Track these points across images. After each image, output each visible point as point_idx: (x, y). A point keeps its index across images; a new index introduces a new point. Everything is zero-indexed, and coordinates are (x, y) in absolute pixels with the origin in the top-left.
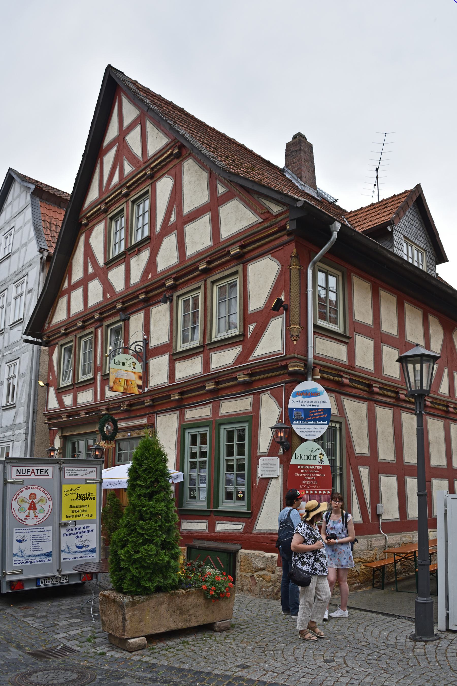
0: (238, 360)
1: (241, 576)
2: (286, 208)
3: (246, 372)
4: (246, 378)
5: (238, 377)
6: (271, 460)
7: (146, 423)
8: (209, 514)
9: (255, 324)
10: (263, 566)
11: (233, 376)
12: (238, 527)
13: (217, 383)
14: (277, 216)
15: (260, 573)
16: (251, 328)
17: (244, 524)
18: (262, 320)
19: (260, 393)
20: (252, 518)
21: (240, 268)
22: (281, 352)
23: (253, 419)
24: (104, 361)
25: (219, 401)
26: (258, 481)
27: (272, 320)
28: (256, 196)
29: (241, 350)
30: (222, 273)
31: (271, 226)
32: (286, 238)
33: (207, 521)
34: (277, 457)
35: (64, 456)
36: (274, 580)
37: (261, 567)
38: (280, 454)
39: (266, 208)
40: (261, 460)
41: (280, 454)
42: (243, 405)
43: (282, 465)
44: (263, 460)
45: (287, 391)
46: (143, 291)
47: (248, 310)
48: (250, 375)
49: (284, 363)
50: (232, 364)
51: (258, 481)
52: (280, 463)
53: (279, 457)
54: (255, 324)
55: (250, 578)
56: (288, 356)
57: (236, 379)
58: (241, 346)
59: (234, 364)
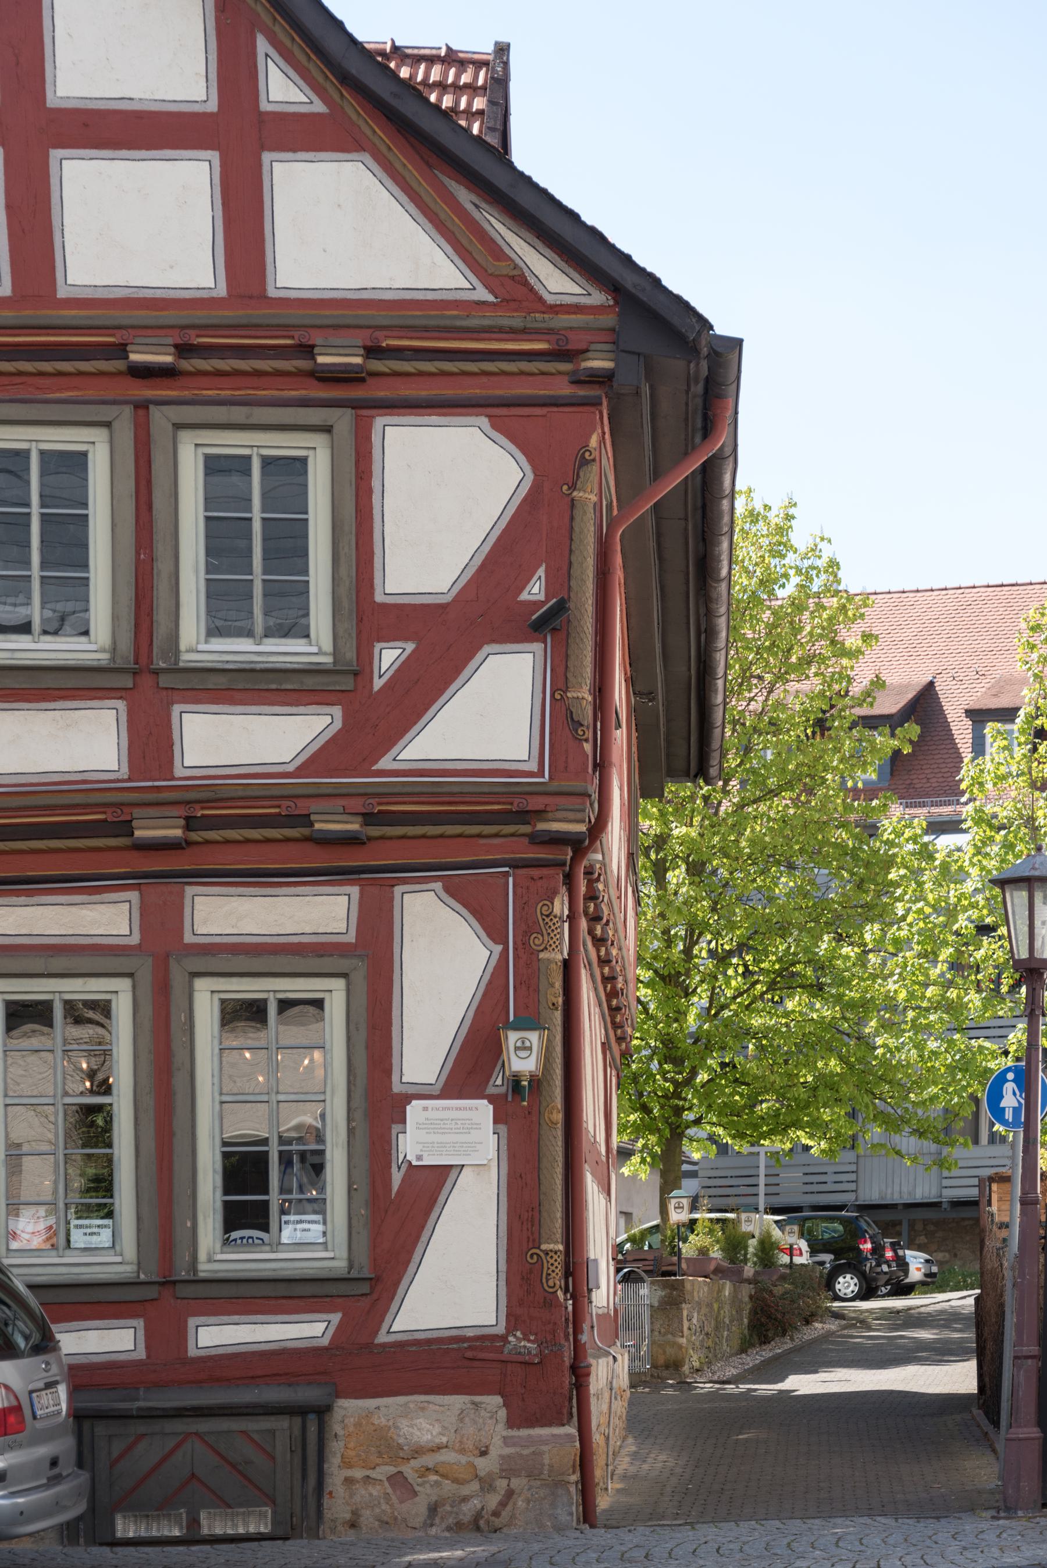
0: (322, 759)
1: (349, 1481)
2: (598, 298)
3: (357, 805)
4: (354, 826)
5: (313, 817)
6: (444, 1109)
8: (152, 1292)
9: (410, 647)
10: (444, 1440)
11: (302, 807)
12: (310, 1330)
13: (190, 823)
14: (557, 309)
15: (429, 1460)
16: (389, 657)
17: (336, 1318)
18: (448, 637)
19: (393, 886)
20: (375, 1296)
21: (343, 420)
22: (533, 766)
23: (371, 960)
24: (473, 799)
25: (180, 885)
26: (397, 1178)
27: (487, 649)
28: (465, 196)
29: (338, 724)
30: (244, 410)
31: (524, 331)
32: (565, 389)
33: (139, 1323)
34: (485, 1102)
35: (702, 1087)
36: (490, 1474)
37: (437, 1440)
38: (490, 1090)
39: (516, 267)
40: (414, 1110)
41: (490, 1090)
42: (324, 912)
43: (503, 1129)
44: (425, 1109)
45: (519, 891)
47: (372, 587)
48: (369, 818)
49: (536, 803)
50: (291, 768)
51: (397, 1178)
52: (496, 1121)
53: (491, 1099)
54: (410, 647)
55: (386, 1484)
56: (555, 786)
57: (305, 820)
58: (337, 711)
59: (302, 770)
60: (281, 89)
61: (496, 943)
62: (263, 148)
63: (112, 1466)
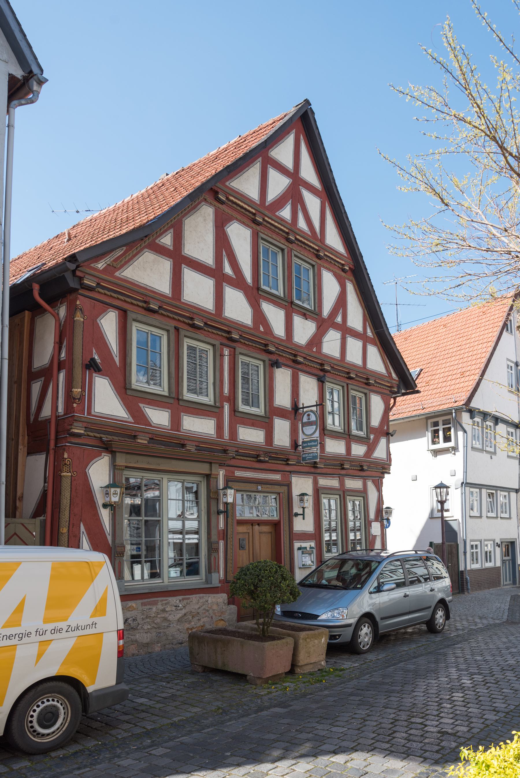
7: (280, 479)
46: (305, 356)
60: (167, 240)
61: (101, 455)
62: (331, 327)
63: (23, 524)
